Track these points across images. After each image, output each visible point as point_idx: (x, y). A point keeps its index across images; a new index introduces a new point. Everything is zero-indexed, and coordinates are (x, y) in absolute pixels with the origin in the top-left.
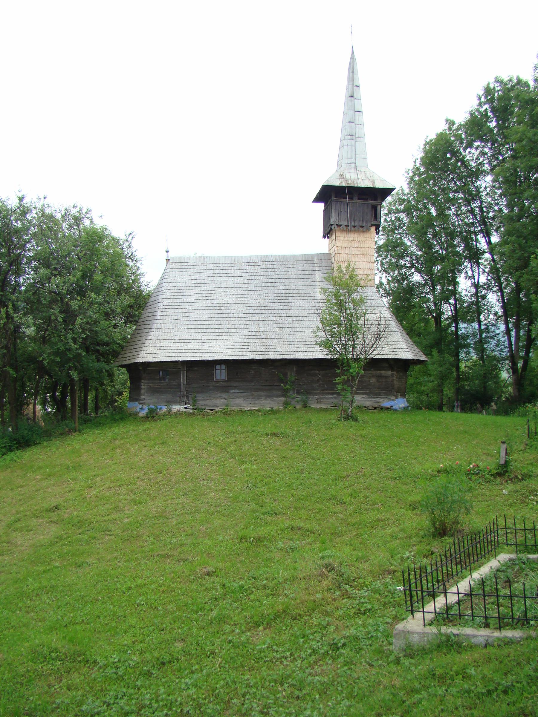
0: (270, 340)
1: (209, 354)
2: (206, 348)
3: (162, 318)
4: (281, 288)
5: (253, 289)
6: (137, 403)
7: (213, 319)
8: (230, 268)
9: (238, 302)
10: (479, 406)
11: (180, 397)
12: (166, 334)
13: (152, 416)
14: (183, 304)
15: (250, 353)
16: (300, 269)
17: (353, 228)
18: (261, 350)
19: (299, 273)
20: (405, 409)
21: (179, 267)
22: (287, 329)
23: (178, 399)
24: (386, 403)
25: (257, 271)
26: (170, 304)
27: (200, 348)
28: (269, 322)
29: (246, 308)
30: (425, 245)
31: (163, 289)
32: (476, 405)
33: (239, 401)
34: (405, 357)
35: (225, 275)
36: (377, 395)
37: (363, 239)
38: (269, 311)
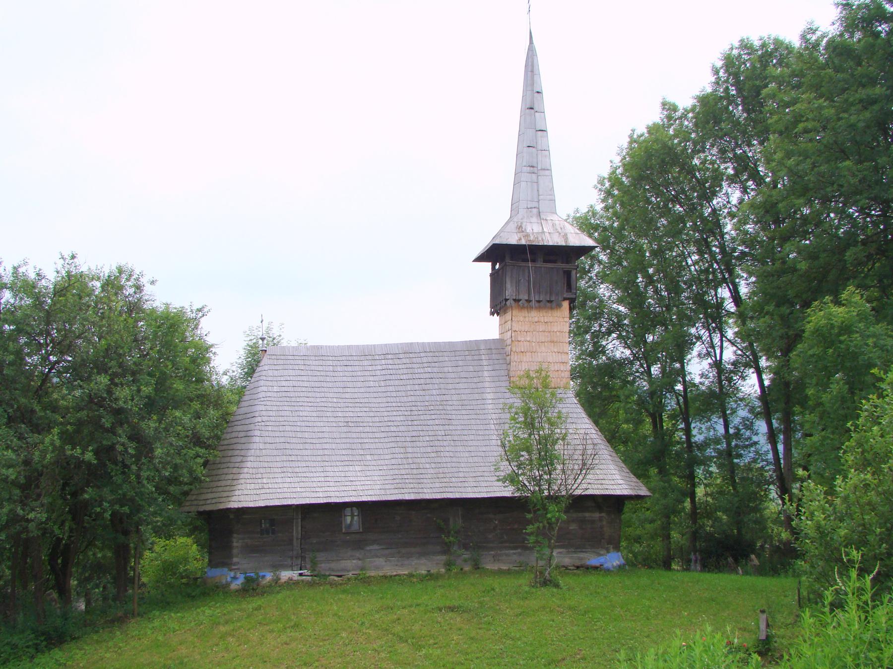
0: (423, 471)
1: (337, 494)
2: (331, 484)
3: (261, 440)
4: (434, 392)
5: (394, 394)
6: (226, 569)
7: (338, 441)
8: (357, 363)
9: (372, 414)
10: (730, 559)
11: (292, 558)
12: (270, 465)
13: (251, 588)
14: (291, 419)
15: (396, 491)
16: (461, 363)
17: (537, 305)
18: (412, 486)
19: (459, 369)
20: (620, 568)
21: (281, 362)
22: (447, 454)
23: (289, 562)
24: (594, 561)
25: (397, 366)
26: (273, 419)
27: (323, 484)
28: (420, 444)
29: (385, 424)
30: (635, 299)
31: (260, 395)
32: (726, 559)
33: (380, 561)
34: (618, 493)
35: (351, 374)
36: (580, 548)
37: (551, 319)
38: (420, 428)
